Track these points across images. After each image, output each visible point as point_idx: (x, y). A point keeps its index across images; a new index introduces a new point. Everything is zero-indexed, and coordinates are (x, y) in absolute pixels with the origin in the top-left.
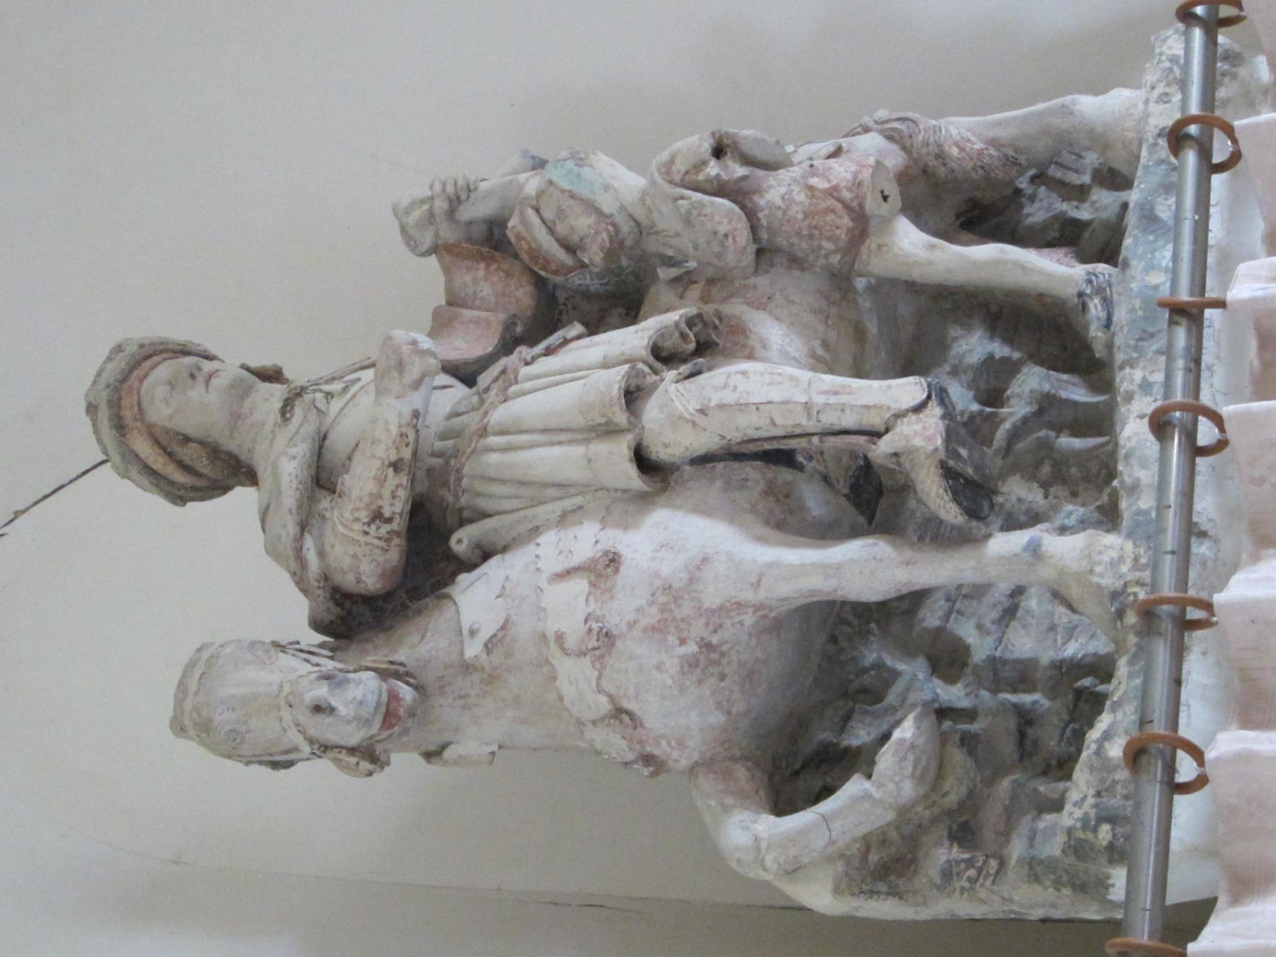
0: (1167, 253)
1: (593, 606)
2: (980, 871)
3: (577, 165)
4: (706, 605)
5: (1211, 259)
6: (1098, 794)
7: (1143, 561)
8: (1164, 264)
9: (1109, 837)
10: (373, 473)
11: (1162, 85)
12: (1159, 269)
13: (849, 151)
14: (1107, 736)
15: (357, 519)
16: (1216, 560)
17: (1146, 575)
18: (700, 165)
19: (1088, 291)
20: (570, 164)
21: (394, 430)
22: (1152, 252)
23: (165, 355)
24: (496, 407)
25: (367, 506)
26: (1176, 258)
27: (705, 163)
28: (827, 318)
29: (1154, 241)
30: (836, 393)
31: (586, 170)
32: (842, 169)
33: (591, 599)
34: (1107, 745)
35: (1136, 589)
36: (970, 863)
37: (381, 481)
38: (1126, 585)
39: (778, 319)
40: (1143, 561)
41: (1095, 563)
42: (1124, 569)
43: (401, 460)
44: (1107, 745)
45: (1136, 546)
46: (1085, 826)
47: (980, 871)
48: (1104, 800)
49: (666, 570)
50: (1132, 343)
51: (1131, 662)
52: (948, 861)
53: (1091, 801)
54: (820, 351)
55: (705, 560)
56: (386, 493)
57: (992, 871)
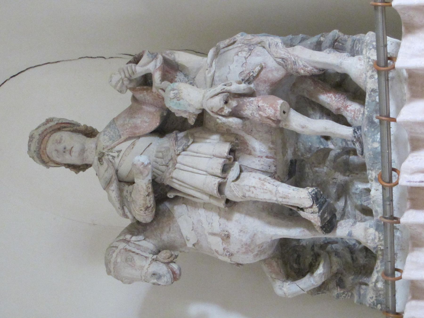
0: (379, 136)
1: (224, 246)
2: (346, 295)
3: (178, 100)
4: (258, 244)
5: (392, 138)
6: (376, 297)
7: (381, 238)
8: (378, 140)
9: (380, 308)
10: (142, 199)
11: (371, 71)
12: (376, 141)
13: (265, 67)
14: (377, 281)
15: (141, 210)
16: (402, 237)
17: (383, 242)
18: (222, 109)
19: (355, 140)
20: (175, 100)
21: (145, 187)
22: (374, 136)
23: (48, 135)
24: (173, 172)
25: (143, 207)
26: (381, 138)
27: (223, 108)
28: (271, 133)
29: (374, 131)
30: (285, 198)
31: (181, 101)
32: (269, 110)
33: (224, 243)
34: (377, 284)
35: (380, 246)
36: (343, 293)
37: (145, 200)
38: (377, 246)
39: (256, 139)
40: (381, 238)
41: (368, 240)
42: (376, 241)
43: (149, 193)
44: (377, 284)
45: (379, 234)
46: (374, 305)
47: (346, 295)
48: (378, 298)
49: (244, 240)
50: (371, 164)
51: (381, 262)
52: (337, 294)
53: (374, 298)
54: (271, 146)
55: (255, 235)
56: (148, 202)
57: (350, 295)
